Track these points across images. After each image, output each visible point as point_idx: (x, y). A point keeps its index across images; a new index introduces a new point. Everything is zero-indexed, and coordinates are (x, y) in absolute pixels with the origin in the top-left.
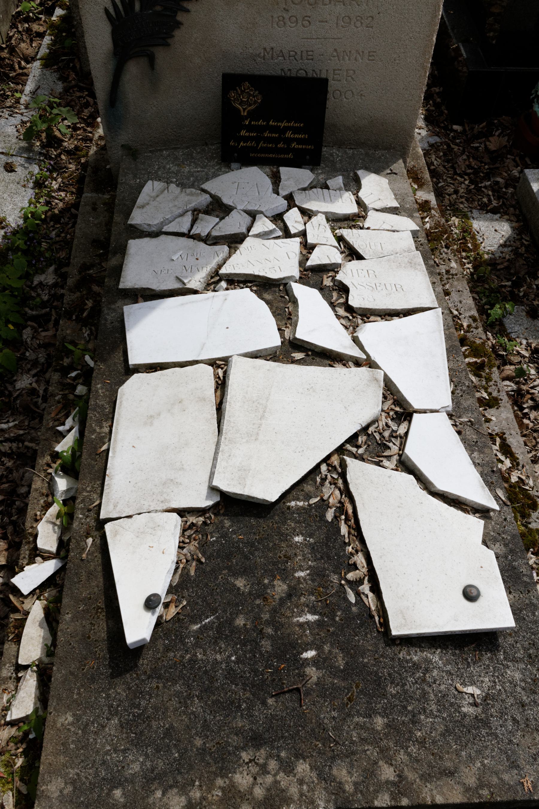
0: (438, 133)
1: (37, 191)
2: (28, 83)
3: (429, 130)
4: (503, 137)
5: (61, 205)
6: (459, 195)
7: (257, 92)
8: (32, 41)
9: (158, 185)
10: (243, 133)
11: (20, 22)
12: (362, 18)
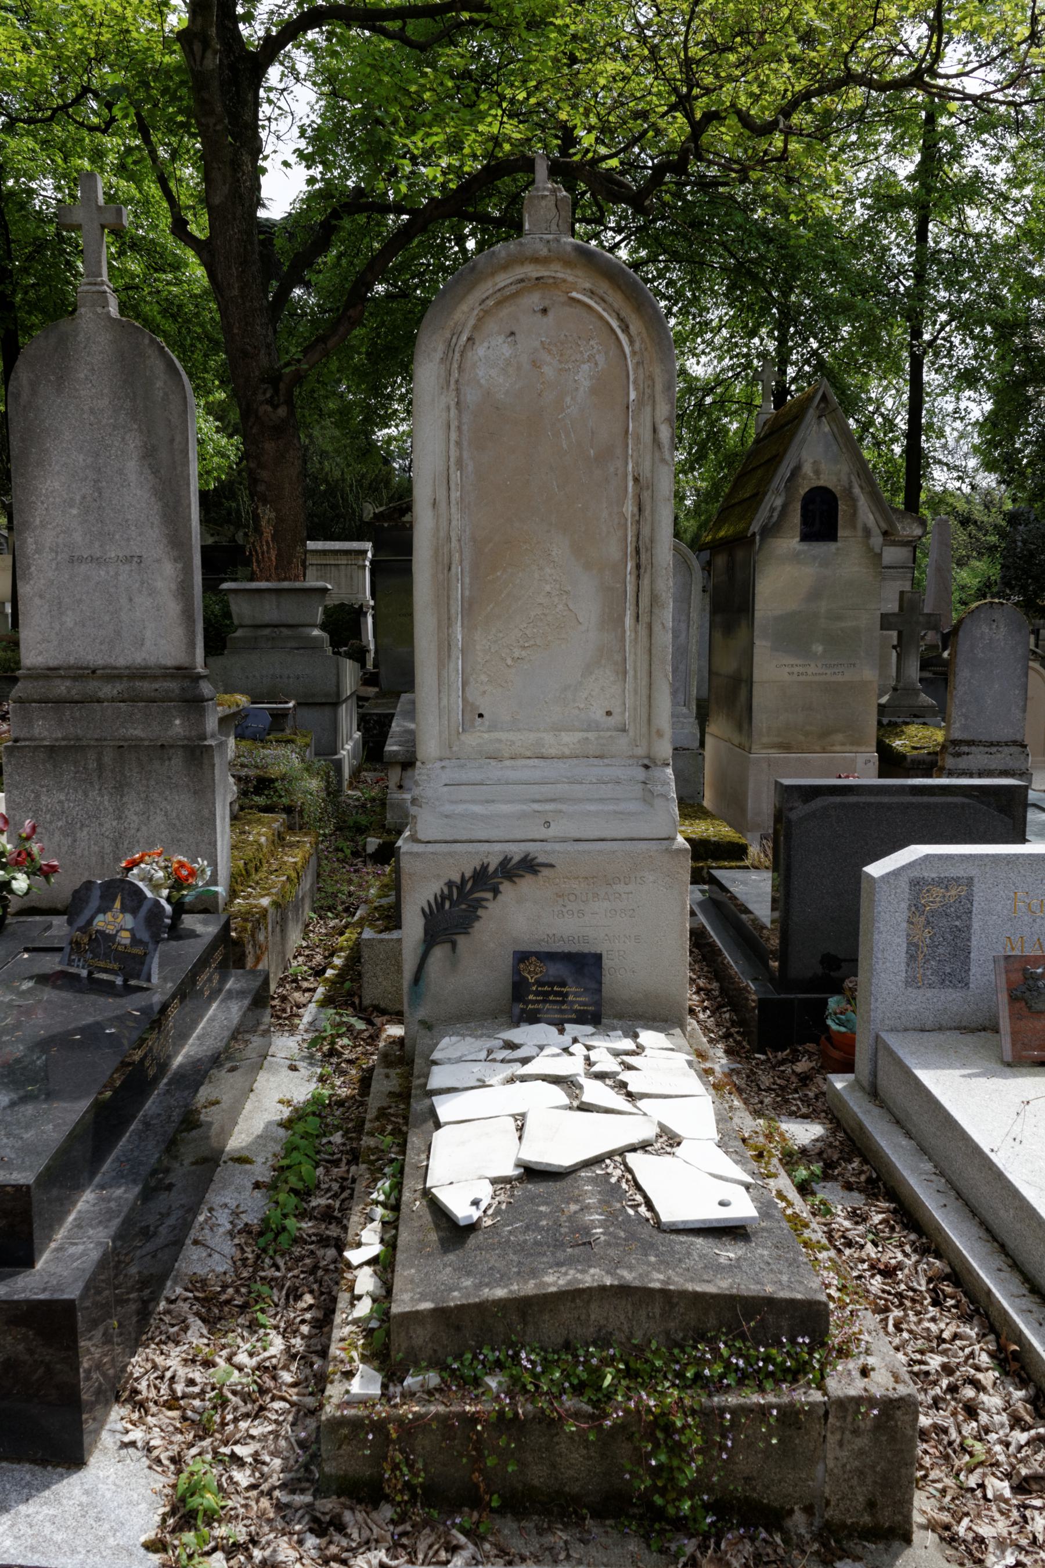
10: (531, 997)
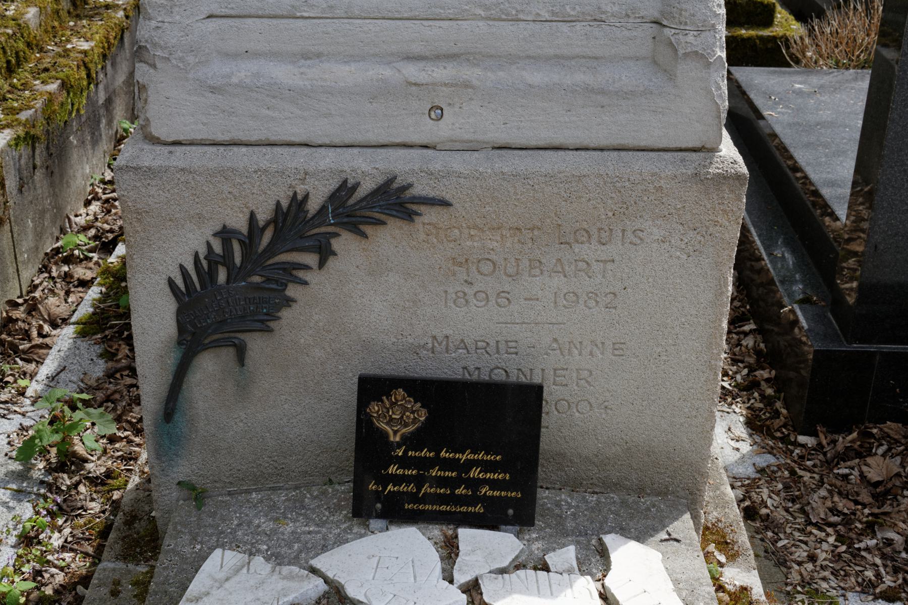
0: (772, 448)
1: (21, 551)
2: (47, 361)
3: (755, 443)
4: (892, 457)
5: (60, 578)
6: (818, 563)
7: (419, 405)
8: (68, 293)
9: (232, 557)
10: (392, 469)
11: (56, 263)
12: (596, 295)
